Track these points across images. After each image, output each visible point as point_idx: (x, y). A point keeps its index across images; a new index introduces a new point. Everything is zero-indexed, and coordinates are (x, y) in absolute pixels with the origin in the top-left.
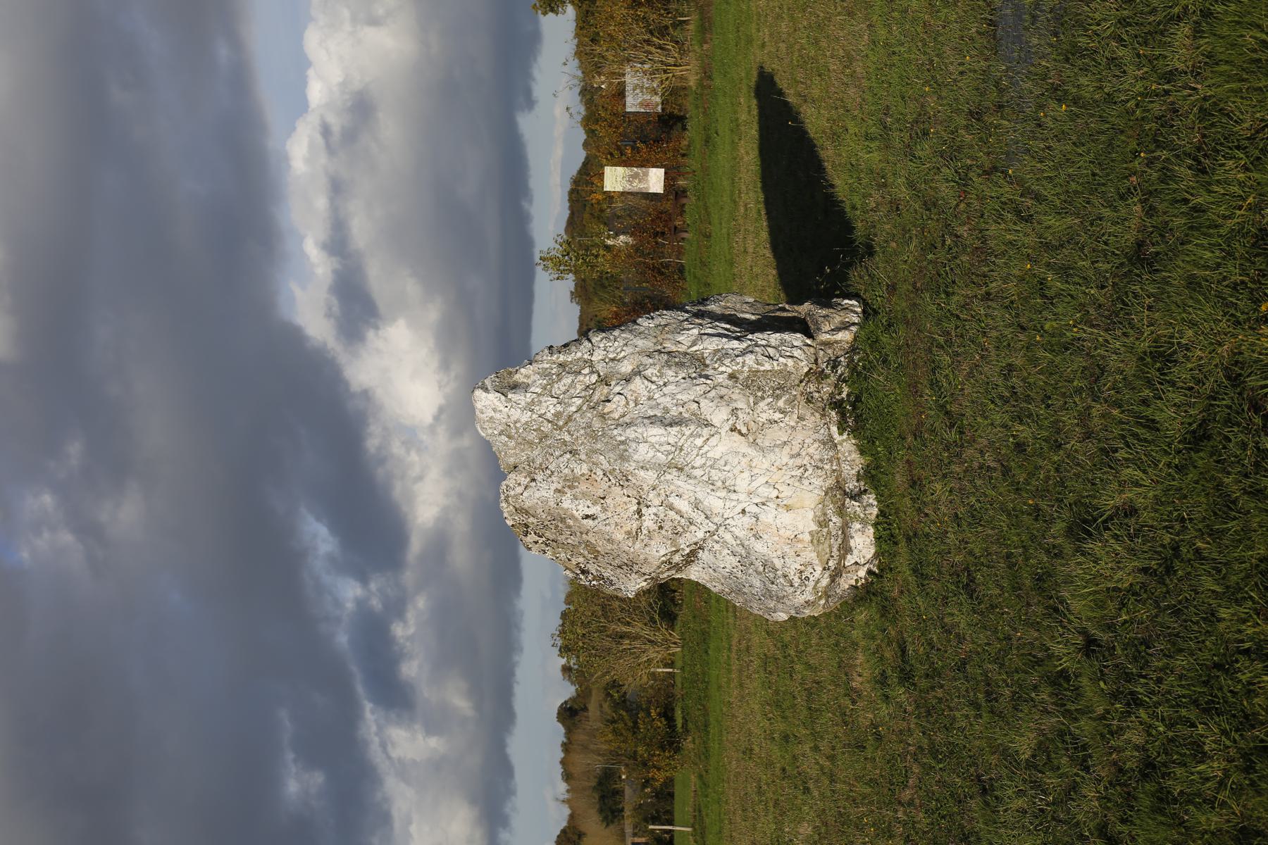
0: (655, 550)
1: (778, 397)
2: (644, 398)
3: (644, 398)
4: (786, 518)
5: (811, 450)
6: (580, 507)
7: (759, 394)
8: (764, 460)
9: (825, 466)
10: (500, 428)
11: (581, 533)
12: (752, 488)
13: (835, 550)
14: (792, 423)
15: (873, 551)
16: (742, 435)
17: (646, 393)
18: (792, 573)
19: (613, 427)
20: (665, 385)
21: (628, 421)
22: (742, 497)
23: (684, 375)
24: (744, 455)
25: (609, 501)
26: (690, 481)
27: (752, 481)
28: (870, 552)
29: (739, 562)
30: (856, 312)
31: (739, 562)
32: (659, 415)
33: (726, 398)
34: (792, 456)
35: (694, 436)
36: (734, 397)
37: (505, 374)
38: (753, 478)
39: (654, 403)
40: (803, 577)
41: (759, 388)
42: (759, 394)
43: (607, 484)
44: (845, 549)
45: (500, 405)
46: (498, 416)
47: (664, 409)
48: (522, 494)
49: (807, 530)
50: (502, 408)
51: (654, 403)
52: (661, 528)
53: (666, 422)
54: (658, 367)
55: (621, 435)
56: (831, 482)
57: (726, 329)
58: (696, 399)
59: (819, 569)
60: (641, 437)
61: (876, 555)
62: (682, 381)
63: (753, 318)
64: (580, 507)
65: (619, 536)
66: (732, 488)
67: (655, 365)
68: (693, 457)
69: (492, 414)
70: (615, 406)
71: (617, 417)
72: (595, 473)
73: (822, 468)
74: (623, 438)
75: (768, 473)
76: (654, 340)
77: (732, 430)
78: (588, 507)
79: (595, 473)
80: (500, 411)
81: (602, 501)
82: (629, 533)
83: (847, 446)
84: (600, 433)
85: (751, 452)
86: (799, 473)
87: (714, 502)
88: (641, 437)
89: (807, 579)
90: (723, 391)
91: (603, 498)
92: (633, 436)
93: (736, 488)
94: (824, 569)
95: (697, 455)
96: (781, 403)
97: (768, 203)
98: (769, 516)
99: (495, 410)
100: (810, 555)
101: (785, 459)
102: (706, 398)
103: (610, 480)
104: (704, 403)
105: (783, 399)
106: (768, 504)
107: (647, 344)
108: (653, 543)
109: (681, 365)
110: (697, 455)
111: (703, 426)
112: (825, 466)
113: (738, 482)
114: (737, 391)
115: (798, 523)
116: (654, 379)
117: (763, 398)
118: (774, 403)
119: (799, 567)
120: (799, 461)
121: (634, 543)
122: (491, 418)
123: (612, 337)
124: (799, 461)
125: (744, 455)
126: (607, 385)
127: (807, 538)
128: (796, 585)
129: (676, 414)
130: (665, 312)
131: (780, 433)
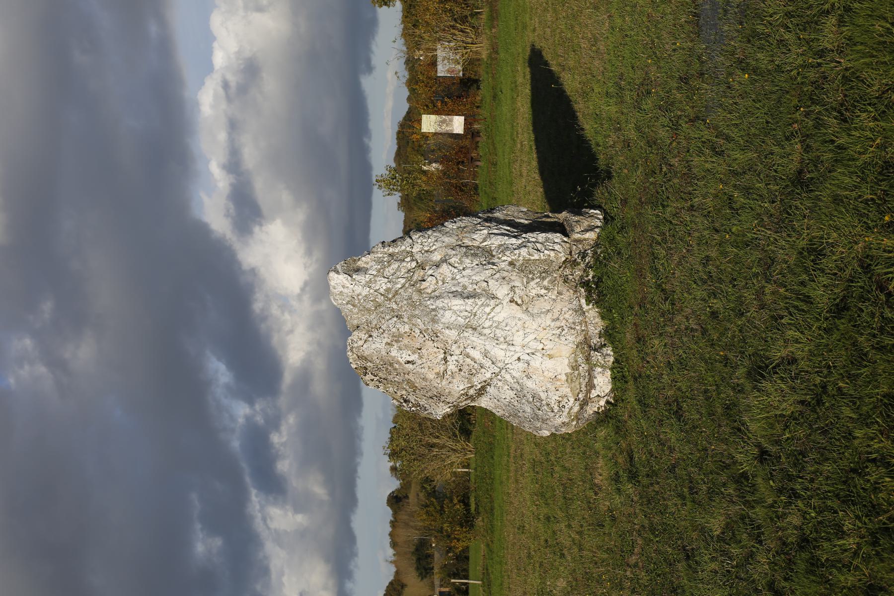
0: (456, 386)
1: (544, 279)
2: (449, 279)
3: (449, 279)
4: (549, 364)
5: (567, 316)
6: (404, 355)
7: (531, 276)
8: (533, 323)
9: (577, 327)
10: (347, 299)
11: (404, 374)
12: (525, 342)
13: (583, 386)
14: (554, 297)
15: (610, 387)
16: (518, 305)
17: (450, 275)
18: (553, 403)
19: (427, 299)
20: (464, 269)
21: (437, 295)
22: (518, 349)
23: (477, 263)
24: (520, 319)
25: (423, 351)
26: (481, 337)
27: (525, 337)
28: (608, 388)
29: (516, 394)
30: (599, 219)
31: (516, 394)
32: (460, 290)
33: (507, 278)
34: (554, 320)
35: (484, 306)
36: (512, 278)
37: (351, 261)
38: (526, 335)
39: (456, 282)
40: (561, 405)
41: (530, 272)
42: (531, 276)
43: (423, 339)
44: (591, 386)
45: (347, 283)
46: (345, 291)
47: (463, 286)
48: (362, 346)
49: (564, 372)
50: (349, 285)
51: (456, 282)
52: (460, 370)
53: (465, 295)
54: (459, 257)
55: (432, 305)
56: (580, 338)
57: (507, 230)
58: (486, 280)
59: (572, 400)
60: (446, 306)
61: (612, 390)
62: (476, 266)
63: (526, 222)
64: (404, 355)
65: (431, 376)
66: (511, 342)
67: (457, 255)
68: (483, 321)
69: (342, 289)
70: (428, 284)
71: (430, 292)
72: (414, 332)
73: (574, 329)
74: (434, 307)
75: (536, 332)
76: (457, 238)
77: (511, 302)
78: (409, 355)
79: (414, 332)
80: (348, 287)
81: (419, 351)
82: (438, 374)
83: (592, 313)
84: (418, 303)
85: (525, 317)
86: (558, 332)
87: (498, 352)
88: (446, 306)
89: (564, 406)
90: (505, 274)
91: (420, 349)
92: (441, 305)
93: (514, 343)
94: (576, 400)
95: (486, 319)
96: (546, 283)
97: (537, 141)
98: (537, 362)
99: (343, 287)
100: (566, 390)
101: (549, 322)
102: (492, 278)
103: (425, 336)
104: (491, 282)
105: (547, 279)
106: (536, 354)
107: (451, 240)
108: (455, 381)
109: (475, 255)
110: (486, 319)
111: (491, 299)
112: (577, 327)
113: (515, 338)
114: (515, 274)
115: (557, 367)
116: (456, 265)
117: (533, 279)
118: (540, 283)
119: (558, 399)
120: (558, 324)
121: (441, 381)
122: (341, 292)
123: (426, 236)
124: (558, 324)
125: (520, 319)
126: (423, 269)
127: (564, 378)
128: (556, 411)
129: (471, 290)
130: (464, 218)
131: (545, 304)
